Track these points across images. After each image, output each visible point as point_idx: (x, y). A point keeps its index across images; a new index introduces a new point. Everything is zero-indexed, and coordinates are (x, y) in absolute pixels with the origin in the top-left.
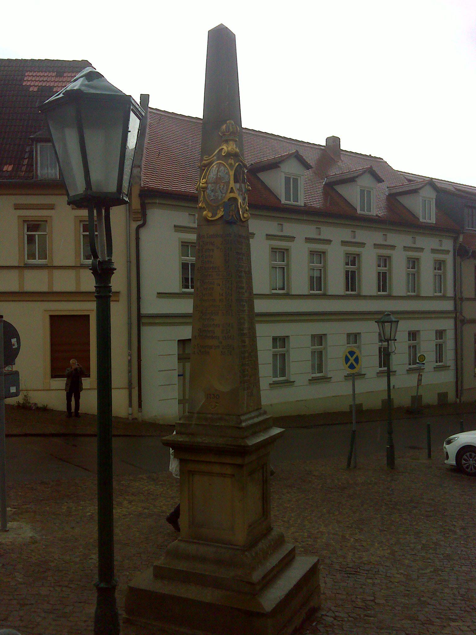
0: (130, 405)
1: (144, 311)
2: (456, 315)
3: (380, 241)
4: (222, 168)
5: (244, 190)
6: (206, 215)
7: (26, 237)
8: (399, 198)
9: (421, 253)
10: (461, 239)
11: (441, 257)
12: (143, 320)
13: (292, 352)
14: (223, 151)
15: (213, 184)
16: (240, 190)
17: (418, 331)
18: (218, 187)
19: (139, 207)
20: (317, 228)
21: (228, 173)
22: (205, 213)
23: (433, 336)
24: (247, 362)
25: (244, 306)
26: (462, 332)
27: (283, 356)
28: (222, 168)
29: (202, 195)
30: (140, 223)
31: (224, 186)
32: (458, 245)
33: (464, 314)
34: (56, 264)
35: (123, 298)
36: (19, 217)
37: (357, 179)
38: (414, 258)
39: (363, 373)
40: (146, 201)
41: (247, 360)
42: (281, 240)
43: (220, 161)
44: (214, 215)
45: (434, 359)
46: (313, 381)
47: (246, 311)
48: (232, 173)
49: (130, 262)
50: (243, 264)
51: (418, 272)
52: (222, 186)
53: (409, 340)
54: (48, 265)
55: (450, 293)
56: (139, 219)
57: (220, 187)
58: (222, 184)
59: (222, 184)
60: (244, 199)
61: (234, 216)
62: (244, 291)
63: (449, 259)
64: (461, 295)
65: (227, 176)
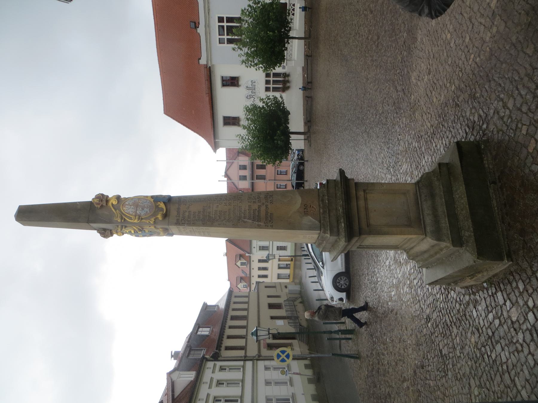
2: (255, 360)
3: (208, 385)
8: (176, 396)
9: (211, 395)
10: (207, 357)
11: (218, 368)
17: (265, 380)
20: (199, 400)
23: (267, 372)
26: (265, 357)
32: (211, 359)
33: (254, 355)
37: (173, 380)
38: (214, 400)
39: (291, 394)
45: (286, 386)
46: (292, 385)
51: (226, 381)
53: (271, 385)
55: (241, 363)
63: (219, 364)
64: (243, 357)
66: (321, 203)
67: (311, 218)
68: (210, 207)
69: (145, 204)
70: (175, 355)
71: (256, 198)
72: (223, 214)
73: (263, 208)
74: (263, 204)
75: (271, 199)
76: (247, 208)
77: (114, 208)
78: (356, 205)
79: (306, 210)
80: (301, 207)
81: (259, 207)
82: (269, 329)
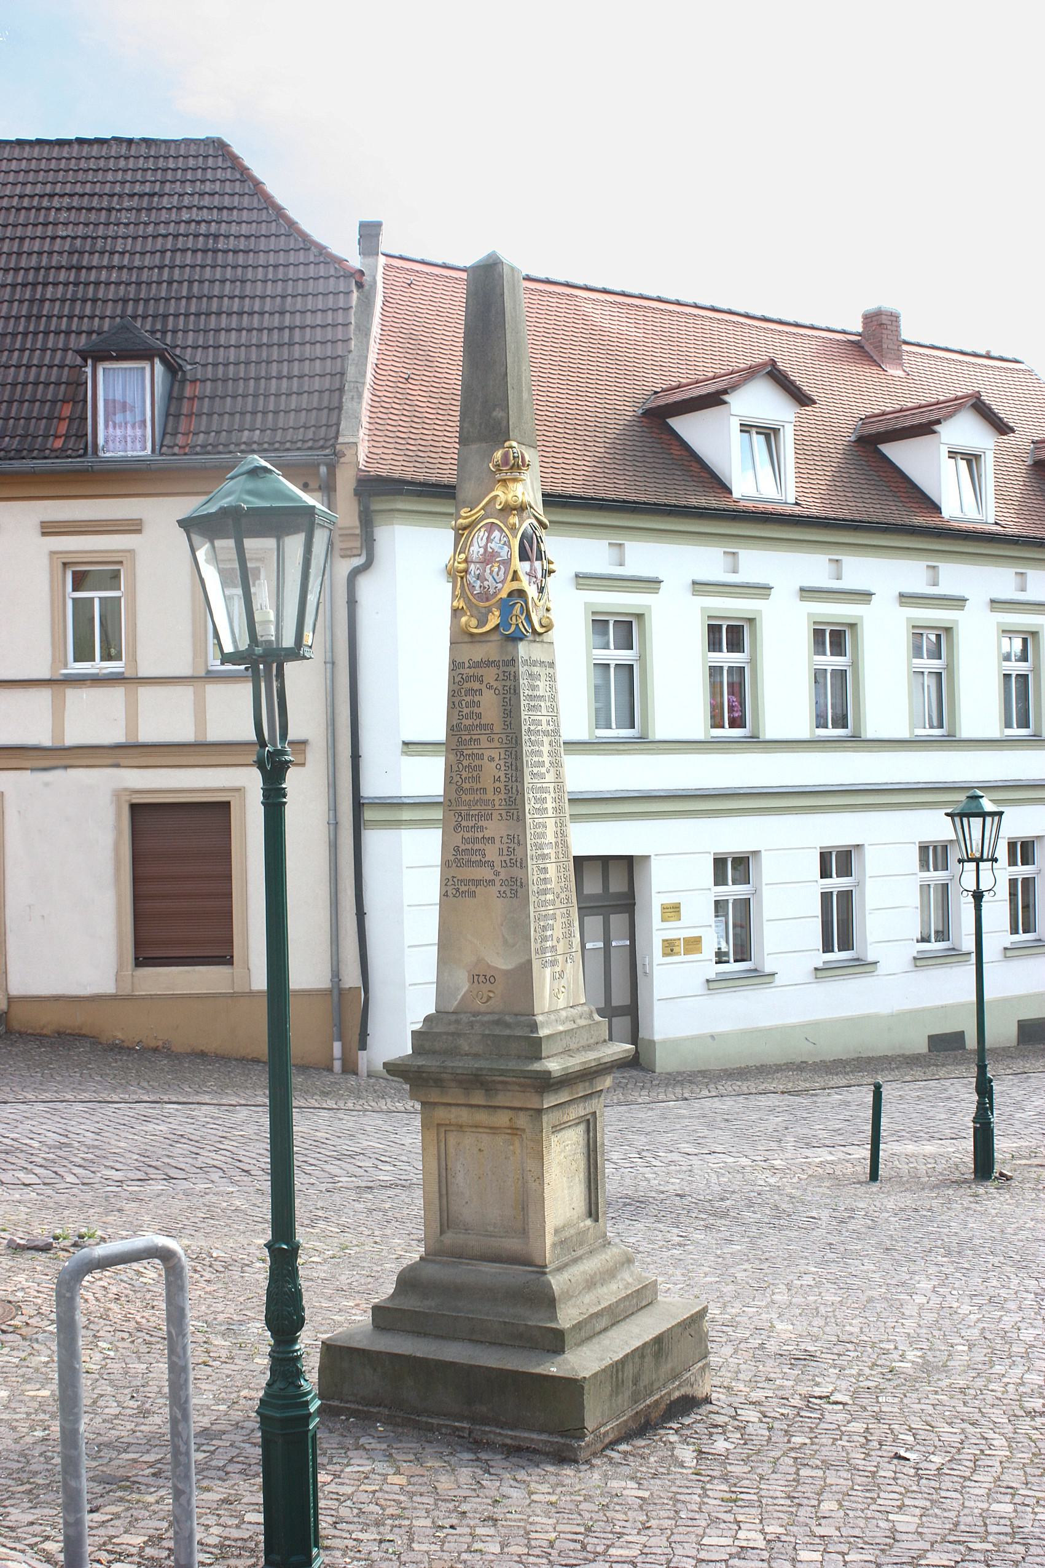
1: (371, 789)
3: (1009, 592)
6: (467, 624)
7: (70, 605)
12: (368, 815)
13: (767, 893)
18: (488, 571)
21: (508, 544)
22: (464, 619)
25: (544, 800)
27: (743, 907)
28: (496, 534)
34: (143, 672)
35: (316, 756)
36: (52, 553)
39: (870, 959)
40: (375, 506)
44: (482, 623)
47: (550, 811)
48: (516, 544)
49: (333, 663)
52: (496, 569)
54: (126, 675)
56: (355, 552)
61: (521, 626)
65: (506, 548)
66: (496, 1017)
67: (464, 990)
68: (491, 741)
69: (491, 579)
72: (475, 774)
73: (486, 873)
74: (497, 874)
75: (509, 895)
76: (488, 834)
77: (487, 504)
78: (459, 1102)
79: (482, 977)
80: (489, 966)
81: (491, 864)
82: (996, 860)
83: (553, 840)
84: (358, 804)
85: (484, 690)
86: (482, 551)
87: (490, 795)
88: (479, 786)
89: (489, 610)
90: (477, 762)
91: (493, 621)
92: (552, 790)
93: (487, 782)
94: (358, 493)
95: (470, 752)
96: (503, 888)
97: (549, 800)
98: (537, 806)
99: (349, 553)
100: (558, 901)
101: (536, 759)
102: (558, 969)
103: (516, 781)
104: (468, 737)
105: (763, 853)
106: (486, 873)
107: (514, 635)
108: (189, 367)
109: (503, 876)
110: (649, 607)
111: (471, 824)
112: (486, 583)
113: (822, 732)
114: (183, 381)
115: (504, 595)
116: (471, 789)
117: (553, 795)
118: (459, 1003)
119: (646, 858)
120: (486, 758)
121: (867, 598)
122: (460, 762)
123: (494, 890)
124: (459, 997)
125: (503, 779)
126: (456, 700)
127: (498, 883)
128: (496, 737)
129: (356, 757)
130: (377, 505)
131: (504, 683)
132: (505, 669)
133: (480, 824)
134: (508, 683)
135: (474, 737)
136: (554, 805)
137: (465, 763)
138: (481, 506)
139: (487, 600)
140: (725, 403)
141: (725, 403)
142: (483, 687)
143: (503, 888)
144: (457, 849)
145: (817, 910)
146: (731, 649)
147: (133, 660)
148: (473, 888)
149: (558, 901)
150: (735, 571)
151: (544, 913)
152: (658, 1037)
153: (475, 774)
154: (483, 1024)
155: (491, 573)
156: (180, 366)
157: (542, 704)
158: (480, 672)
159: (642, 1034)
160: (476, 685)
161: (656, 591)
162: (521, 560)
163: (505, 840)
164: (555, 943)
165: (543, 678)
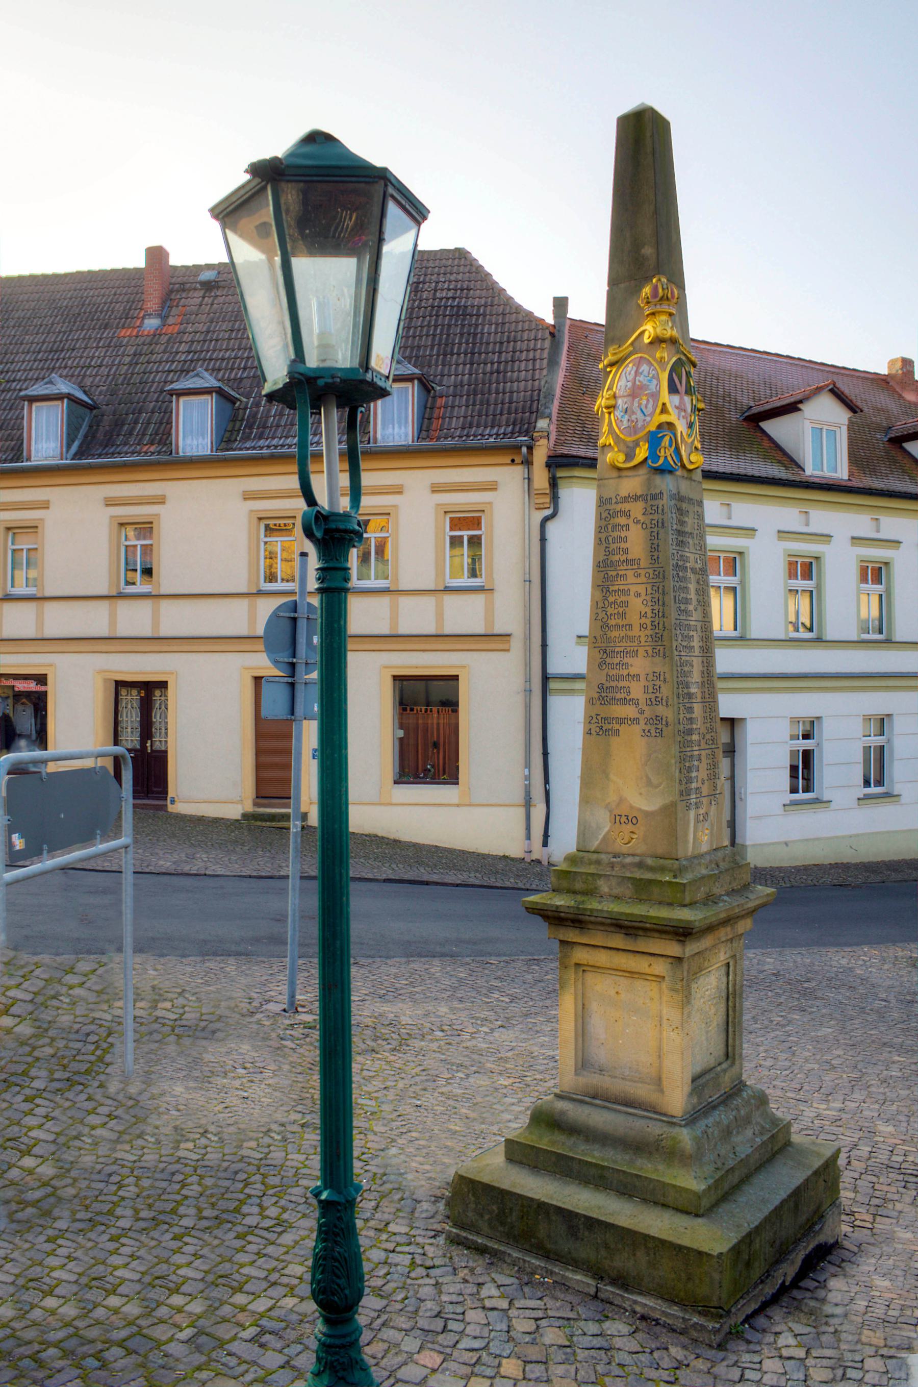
0: (528, 837)
1: (552, 669)
4: (644, 368)
5: (689, 410)
12: (552, 685)
13: (826, 745)
14: (646, 335)
15: (625, 400)
16: (679, 408)
18: (636, 404)
19: (547, 485)
24: (696, 753)
29: (607, 421)
30: (548, 512)
31: (648, 401)
39: (895, 793)
40: (558, 475)
41: (697, 748)
42: (804, 541)
43: (640, 355)
48: (664, 377)
50: (688, 555)
52: (644, 402)
56: (547, 506)
57: (640, 405)
58: (645, 398)
59: (645, 398)
60: (690, 425)
61: (669, 459)
62: (691, 608)
66: (637, 859)
67: (606, 830)
69: (639, 413)
70: (156, 255)
71: (658, 694)
72: (621, 610)
73: (629, 711)
74: (642, 712)
75: (654, 734)
76: (633, 671)
80: (632, 807)
83: (699, 680)
84: (546, 678)
85: (632, 526)
86: (629, 384)
87: (636, 631)
88: (625, 622)
89: (637, 444)
90: (623, 598)
91: (642, 453)
92: (699, 628)
93: (635, 620)
94: (548, 465)
95: (616, 588)
96: (647, 728)
97: (696, 639)
98: (685, 644)
99: (542, 506)
100: (703, 742)
101: (682, 595)
102: (701, 811)
103: (663, 616)
104: (614, 573)
105: (824, 718)
106: (629, 711)
107: (663, 468)
108: (438, 388)
109: (647, 714)
110: (748, 548)
111: (616, 661)
112: (633, 417)
113: (865, 636)
114: (434, 397)
115: (653, 428)
116: (617, 625)
117: (699, 633)
118: (600, 843)
119: (743, 720)
120: (632, 594)
121: (897, 545)
122: (605, 598)
123: (637, 729)
124: (601, 837)
125: (649, 614)
126: (603, 536)
127: (642, 722)
128: (643, 572)
129: (544, 645)
130: (560, 474)
131: (651, 517)
132: (653, 503)
133: (624, 661)
134: (656, 517)
135: (621, 573)
136: (701, 644)
137: (611, 599)
138: (630, 341)
139: (635, 433)
140: (800, 410)
141: (800, 410)
142: (630, 522)
143: (647, 728)
144: (601, 687)
145: (860, 758)
146: (804, 578)
147: (396, 580)
148: (617, 726)
149: (703, 742)
150: (807, 525)
151: (689, 754)
152: (748, 843)
153: (621, 610)
154: (624, 866)
155: (640, 405)
156: (433, 387)
157: (691, 541)
158: (626, 506)
159: (738, 840)
160: (622, 521)
161: (752, 537)
162: (669, 393)
163: (650, 677)
164: (699, 785)
165: (691, 515)
